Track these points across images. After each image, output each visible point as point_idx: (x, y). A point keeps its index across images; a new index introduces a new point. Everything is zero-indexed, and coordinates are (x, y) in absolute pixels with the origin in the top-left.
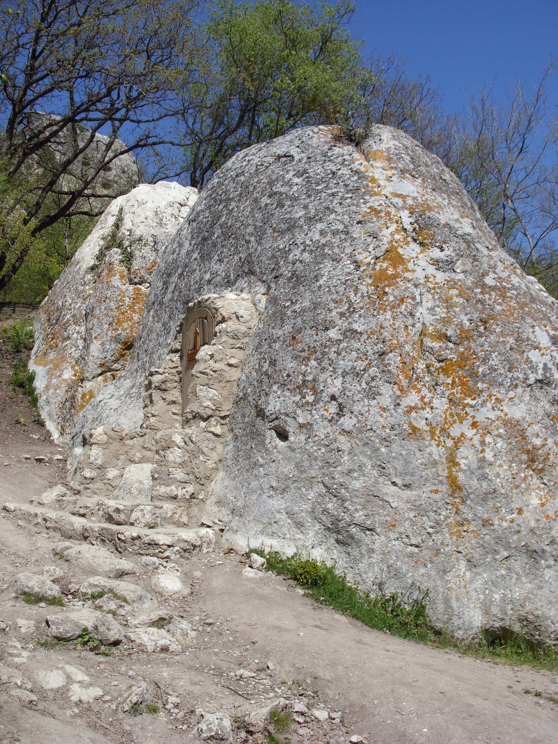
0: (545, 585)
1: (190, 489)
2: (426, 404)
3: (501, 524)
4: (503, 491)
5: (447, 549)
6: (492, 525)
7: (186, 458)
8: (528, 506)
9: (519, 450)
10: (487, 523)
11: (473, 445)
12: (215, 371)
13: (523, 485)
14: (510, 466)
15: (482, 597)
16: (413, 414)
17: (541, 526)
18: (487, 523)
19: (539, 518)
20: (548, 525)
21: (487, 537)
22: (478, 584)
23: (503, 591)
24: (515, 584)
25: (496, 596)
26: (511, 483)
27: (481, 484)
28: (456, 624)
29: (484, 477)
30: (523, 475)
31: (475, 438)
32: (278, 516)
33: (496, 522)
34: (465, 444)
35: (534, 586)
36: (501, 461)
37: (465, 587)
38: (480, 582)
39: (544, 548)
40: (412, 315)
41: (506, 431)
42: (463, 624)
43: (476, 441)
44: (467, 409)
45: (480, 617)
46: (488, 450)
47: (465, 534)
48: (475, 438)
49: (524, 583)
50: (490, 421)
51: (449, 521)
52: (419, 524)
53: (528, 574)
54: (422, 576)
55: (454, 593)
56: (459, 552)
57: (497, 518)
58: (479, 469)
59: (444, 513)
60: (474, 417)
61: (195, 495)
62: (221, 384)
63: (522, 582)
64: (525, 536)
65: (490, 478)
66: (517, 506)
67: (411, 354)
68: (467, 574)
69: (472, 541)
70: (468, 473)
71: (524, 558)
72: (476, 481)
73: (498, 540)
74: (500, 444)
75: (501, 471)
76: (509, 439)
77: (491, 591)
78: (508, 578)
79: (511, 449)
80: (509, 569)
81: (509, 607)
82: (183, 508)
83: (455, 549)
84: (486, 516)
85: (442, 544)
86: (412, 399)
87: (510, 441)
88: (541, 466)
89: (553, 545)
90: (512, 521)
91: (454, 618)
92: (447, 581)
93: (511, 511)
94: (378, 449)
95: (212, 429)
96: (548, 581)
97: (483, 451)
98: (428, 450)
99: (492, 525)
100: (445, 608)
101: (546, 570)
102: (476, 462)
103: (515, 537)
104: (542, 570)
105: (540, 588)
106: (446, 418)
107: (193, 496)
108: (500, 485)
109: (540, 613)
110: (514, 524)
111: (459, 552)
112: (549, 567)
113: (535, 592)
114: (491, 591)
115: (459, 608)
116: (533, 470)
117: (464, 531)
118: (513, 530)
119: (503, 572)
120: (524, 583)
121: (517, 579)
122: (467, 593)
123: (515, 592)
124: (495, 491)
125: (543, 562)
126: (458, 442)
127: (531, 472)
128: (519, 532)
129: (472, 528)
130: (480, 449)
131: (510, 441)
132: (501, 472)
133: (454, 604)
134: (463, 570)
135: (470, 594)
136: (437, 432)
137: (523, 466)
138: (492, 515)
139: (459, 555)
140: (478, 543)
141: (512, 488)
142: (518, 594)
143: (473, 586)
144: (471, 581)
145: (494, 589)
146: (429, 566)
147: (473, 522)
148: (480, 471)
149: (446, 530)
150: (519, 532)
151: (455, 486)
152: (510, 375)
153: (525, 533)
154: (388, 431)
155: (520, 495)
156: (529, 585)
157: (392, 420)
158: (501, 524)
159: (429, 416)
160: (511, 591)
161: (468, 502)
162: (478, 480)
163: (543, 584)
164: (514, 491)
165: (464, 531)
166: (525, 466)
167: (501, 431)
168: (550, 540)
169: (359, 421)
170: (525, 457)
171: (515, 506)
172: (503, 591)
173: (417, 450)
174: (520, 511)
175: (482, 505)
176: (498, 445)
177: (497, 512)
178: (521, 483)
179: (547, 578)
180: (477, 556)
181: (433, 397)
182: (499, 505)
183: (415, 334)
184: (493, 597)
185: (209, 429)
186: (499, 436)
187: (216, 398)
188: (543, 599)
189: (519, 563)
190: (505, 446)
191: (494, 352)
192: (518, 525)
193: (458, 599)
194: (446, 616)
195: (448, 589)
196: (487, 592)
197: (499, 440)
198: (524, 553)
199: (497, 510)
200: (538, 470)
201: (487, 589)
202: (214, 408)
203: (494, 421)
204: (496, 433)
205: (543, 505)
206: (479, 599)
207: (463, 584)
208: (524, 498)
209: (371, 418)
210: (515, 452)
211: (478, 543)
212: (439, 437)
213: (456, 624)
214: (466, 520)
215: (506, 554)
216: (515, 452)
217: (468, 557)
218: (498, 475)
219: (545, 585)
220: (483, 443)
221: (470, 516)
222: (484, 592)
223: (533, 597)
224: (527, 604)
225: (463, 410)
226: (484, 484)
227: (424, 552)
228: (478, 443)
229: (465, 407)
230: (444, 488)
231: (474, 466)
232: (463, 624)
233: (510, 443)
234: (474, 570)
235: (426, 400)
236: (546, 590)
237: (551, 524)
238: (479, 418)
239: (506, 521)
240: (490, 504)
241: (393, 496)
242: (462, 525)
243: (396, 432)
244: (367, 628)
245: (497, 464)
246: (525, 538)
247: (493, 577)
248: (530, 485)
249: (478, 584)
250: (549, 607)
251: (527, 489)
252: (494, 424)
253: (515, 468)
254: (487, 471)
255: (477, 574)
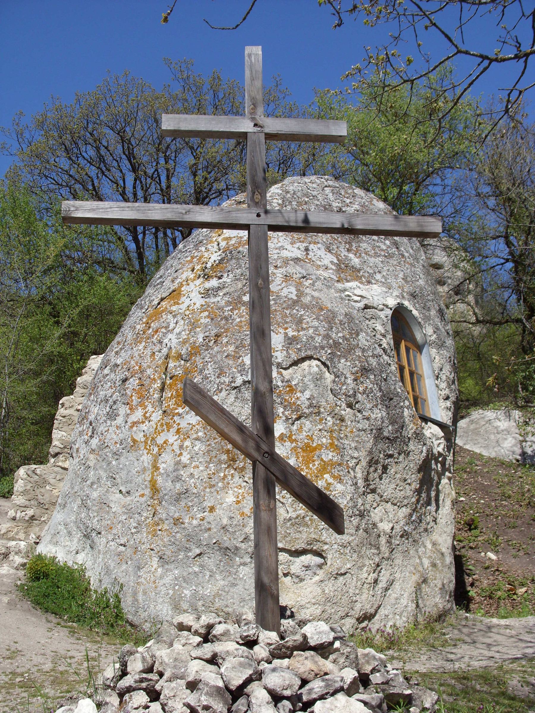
0: (239, 582)
1: (30, 512)
2: (147, 418)
3: (191, 522)
4: (195, 491)
5: (143, 547)
6: (182, 523)
7: (28, 487)
8: (222, 504)
9: (219, 450)
10: (177, 522)
11: (173, 450)
12: (64, 417)
13: (220, 484)
14: (207, 467)
15: (171, 592)
16: (135, 428)
17: (235, 523)
18: (177, 522)
19: (233, 515)
20: (241, 522)
21: (178, 535)
22: (168, 580)
23: (194, 588)
24: (209, 581)
25: (186, 592)
26: (205, 482)
27: (175, 485)
28: (142, 617)
29: (178, 479)
30: (222, 475)
31: (175, 443)
32: (60, 527)
33: (187, 521)
34: (167, 450)
35: (226, 583)
36: (197, 463)
37: (154, 582)
38: (170, 577)
39: (237, 545)
40: (160, 342)
41: (205, 433)
42: (149, 616)
43: (176, 447)
44: (175, 418)
45: (170, 612)
46: (185, 454)
47: (159, 532)
48: (175, 443)
49: (218, 580)
50: (191, 426)
51: (148, 521)
52: (127, 526)
53: (222, 571)
54: (123, 573)
55: (142, 587)
56: (152, 550)
57: (188, 516)
58: (174, 471)
59: (145, 514)
60: (179, 424)
61: (35, 517)
62: (70, 427)
63: (216, 579)
64: (215, 533)
65: (183, 479)
66: (209, 505)
67: (152, 377)
68: (159, 570)
69: (165, 540)
70: (165, 476)
71: (218, 556)
72: (170, 483)
73: (189, 538)
74: (198, 446)
75: (196, 473)
76: (208, 441)
77: (181, 586)
78: (201, 575)
79: (208, 451)
80: (201, 566)
81: (200, 603)
82: (20, 527)
83: (149, 547)
84: (177, 515)
85: (140, 542)
86: (138, 414)
87: (208, 443)
88: (242, 464)
89: (248, 542)
90: (203, 519)
91: (141, 611)
92: (139, 576)
93: (204, 510)
94: (111, 463)
95: (60, 464)
96: (242, 578)
97: (181, 454)
98: (141, 459)
99: (182, 523)
100: (133, 601)
101: (241, 567)
102: (173, 466)
103: (206, 535)
104: (235, 567)
105: (234, 585)
106: (156, 429)
107: (32, 518)
108: (193, 485)
109: (230, 610)
110: (205, 522)
111: (152, 550)
112: (245, 564)
113: (227, 589)
114: (181, 586)
115: (144, 601)
116: (235, 469)
117: (160, 530)
118: (203, 528)
119: (196, 569)
120: (218, 580)
121: (211, 576)
122: (156, 587)
123: (207, 589)
124: (187, 491)
125: (237, 559)
126: (162, 448)
127: (232, 471)
128: (209, 529)
129: (166, 527)
130: (179, 452)
131: (208, 443)
132: (195, 473)
133: (140, 597)
134: (155, 566)
135: (158, 589)
136: (149, 442)
137: (223, 466)
138: (183, 514)
139: (152, 552)
140: (170, 541)
141: (205, 488)
142: (209, 591)
143: (162, 582)
144: (161, 577)
145: (184, 585)
146: (129, 563)
147: (166, 522)
148: (175, 474)
149: (145, 530)
150: (209, 529)
151: (155, 489)
152: (218, 381)
153: (215, 530)
154: (118, 446)
155: (215, 493)
156: (222, 583)
157: (121, 436)
158: (191, 522)
159: (145, 428)
160: (203, 587)
161: (163, 503)
162: (172, 482)
163: (238, 582)
164: (208, 490)
165: (160, 530)
166: (226, 466)
167: (200, 434)
168: (243, 536)
169: (100, 440)
170: (224, 457)
171: (207, 504)
172: (194, 588)
173: (135, 460)
174: (212, 509)
175: (175, 505)
176: (196, 449)
177: (188, 511)
178: (218, 483)
179: (241, 576)
180: (168, 553)
181: (154, 412)
182: (191, 504)
183: (160, 358)
184: (183, 592)
185: (57, 464)
186: (197, 439)
187: (64, 438)
188: (235, 596)
189: (211, 561)
190: (203, 448)
191: (210, 362)
192: (209, 523)
193: (145, 593)
194: (134, 609)
195: (137, 583)
196: (177, 588)
197: (197, 442)
198: (217, 550)
199: (188, 509)
200: (239, 469)
201: (177, 585)
202: (62, 446)
203: (194, 426)
204: (195, 436)
205: (238, 502)
206: (168, 594)
207: (153, 579)
208: (219, 497)
209: (108, 436)
210: (213, 454)
211: (170, 541)
212: (150, 446)
213: (142, 617)
214: (161, 519)
215: (198, 551)
216: (213, 454)
217: (160, 554)
218: (192, 475)
219: (239, 582)
220: (181, 447)
221: (164, 516)
222: (174, 587)
223: (224, 594)
224: (217, 600)
225: (172, 419)
226: (178, 486)
227: (128, 550)
228: (178, 447)
229: (174, 416)
230: (147, 492)
231: (171, 469)
232: (149, 616)
233: (209, 445)
234: (166, 567)
235: (148, 415)
236: (240, 587)
237: (245, 521)
238: (183, 424)
239: (196, 519)
240: (183, 504)
241: (115, 502)
242: (158, 524)
243: (123, 446)
244: (39, 612)
245: (193, 465)
246: (216, 535)
247: (185, 574)
248: (228, 483)
249: (168, 580)
250: (242, 604)
251: (224, 488)
252: (195, 428)
253: (213, 468)
254: (182, 473)
255: (167, 570)
